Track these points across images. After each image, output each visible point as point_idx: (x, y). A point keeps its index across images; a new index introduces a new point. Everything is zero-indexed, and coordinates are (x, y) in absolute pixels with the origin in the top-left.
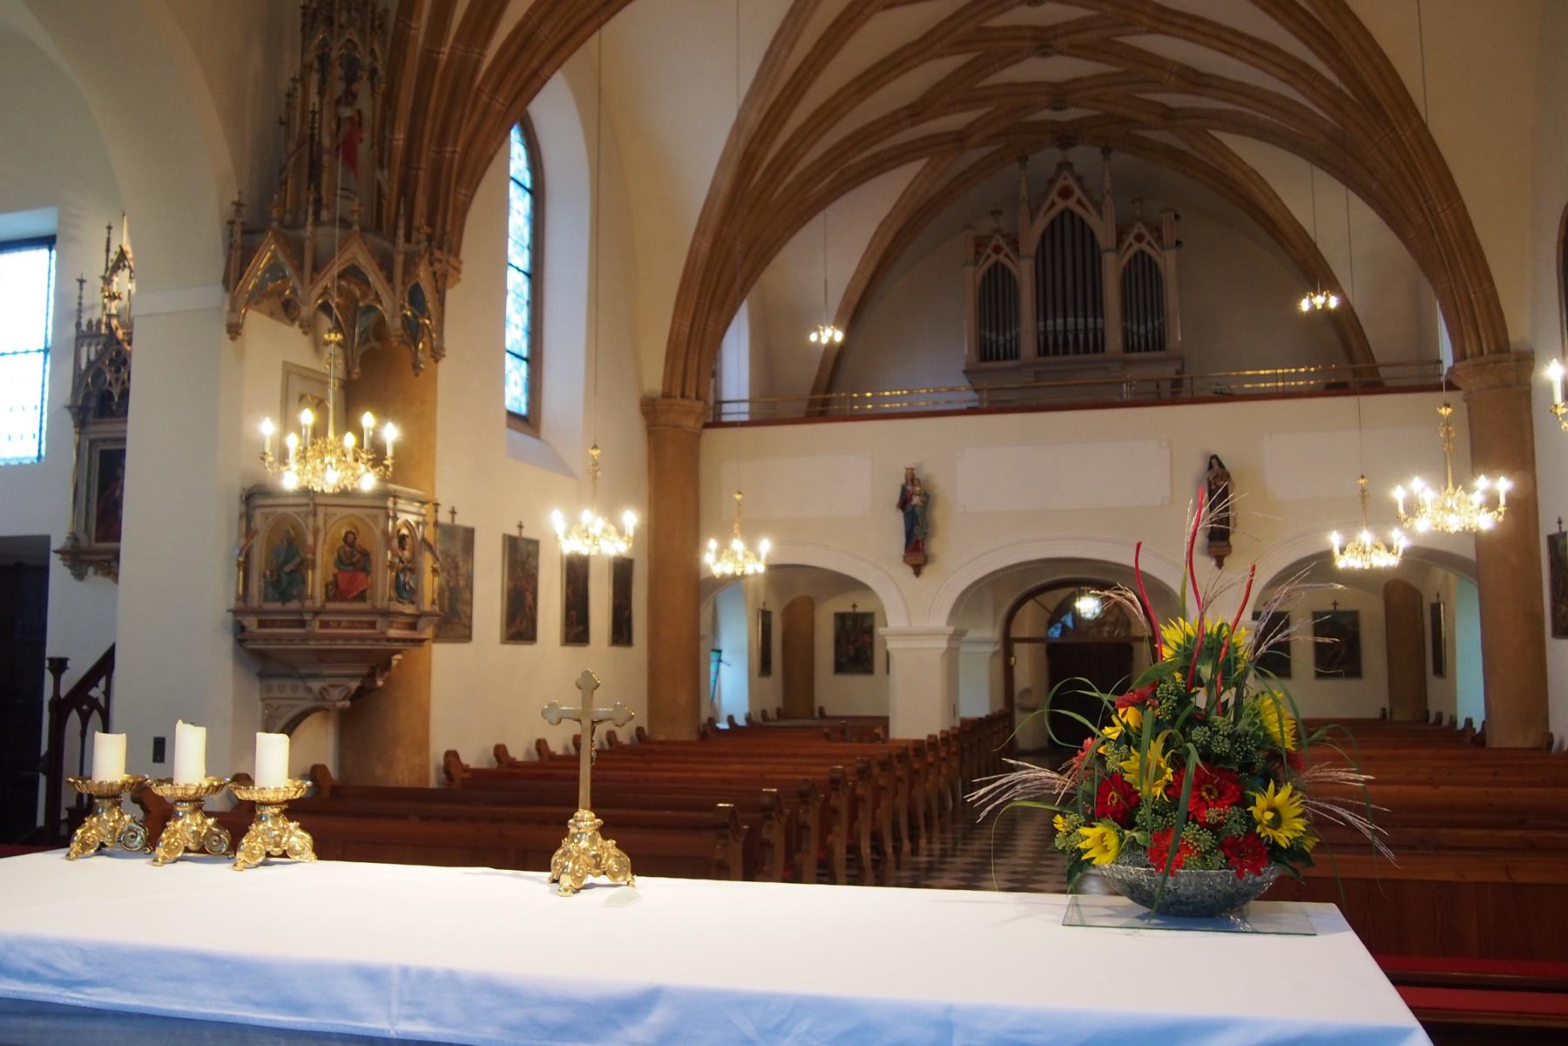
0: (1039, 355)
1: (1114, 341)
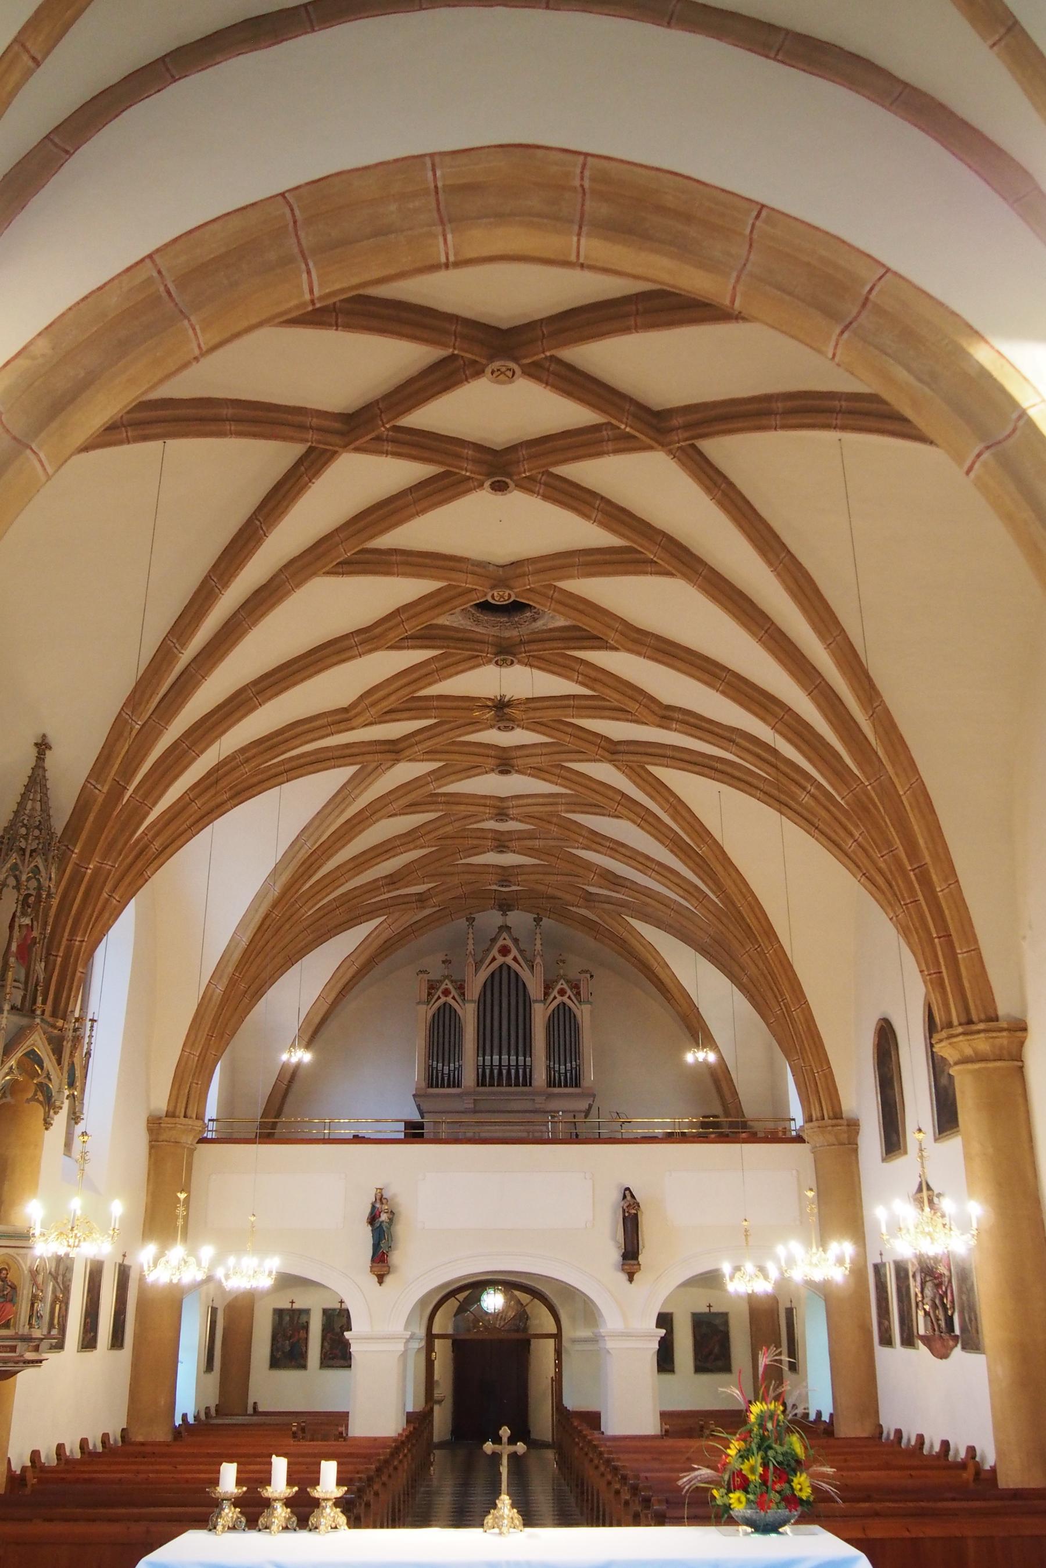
0: (430, 1085)
1: (540, 1077)
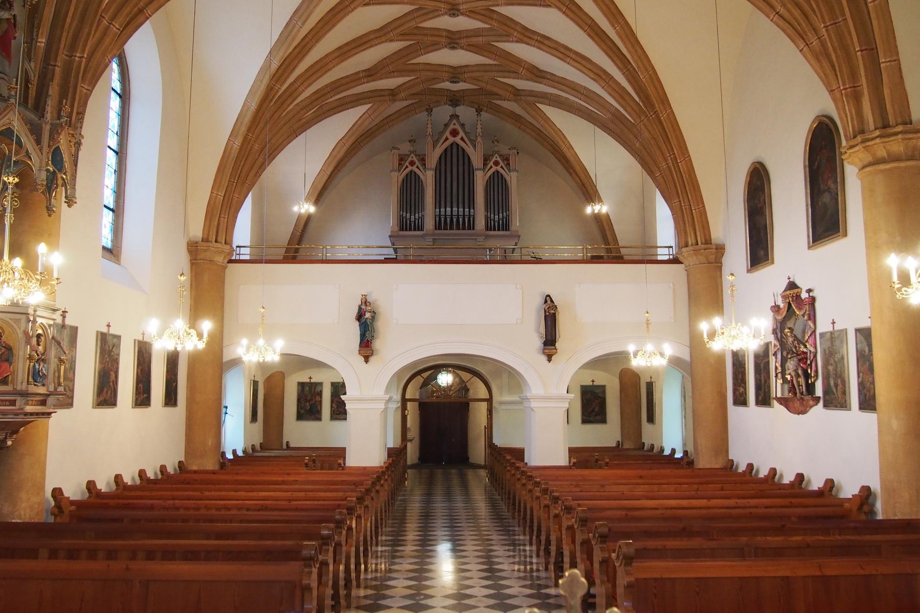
0: (402, 229)
1: (480, 223)
